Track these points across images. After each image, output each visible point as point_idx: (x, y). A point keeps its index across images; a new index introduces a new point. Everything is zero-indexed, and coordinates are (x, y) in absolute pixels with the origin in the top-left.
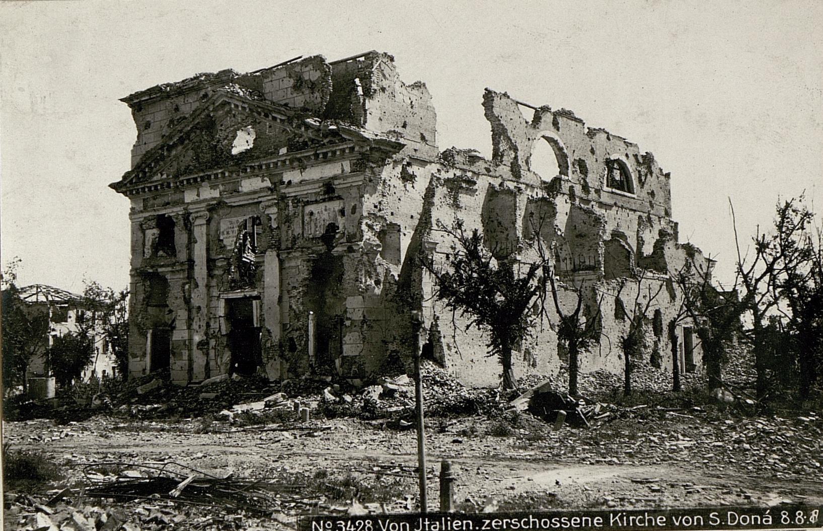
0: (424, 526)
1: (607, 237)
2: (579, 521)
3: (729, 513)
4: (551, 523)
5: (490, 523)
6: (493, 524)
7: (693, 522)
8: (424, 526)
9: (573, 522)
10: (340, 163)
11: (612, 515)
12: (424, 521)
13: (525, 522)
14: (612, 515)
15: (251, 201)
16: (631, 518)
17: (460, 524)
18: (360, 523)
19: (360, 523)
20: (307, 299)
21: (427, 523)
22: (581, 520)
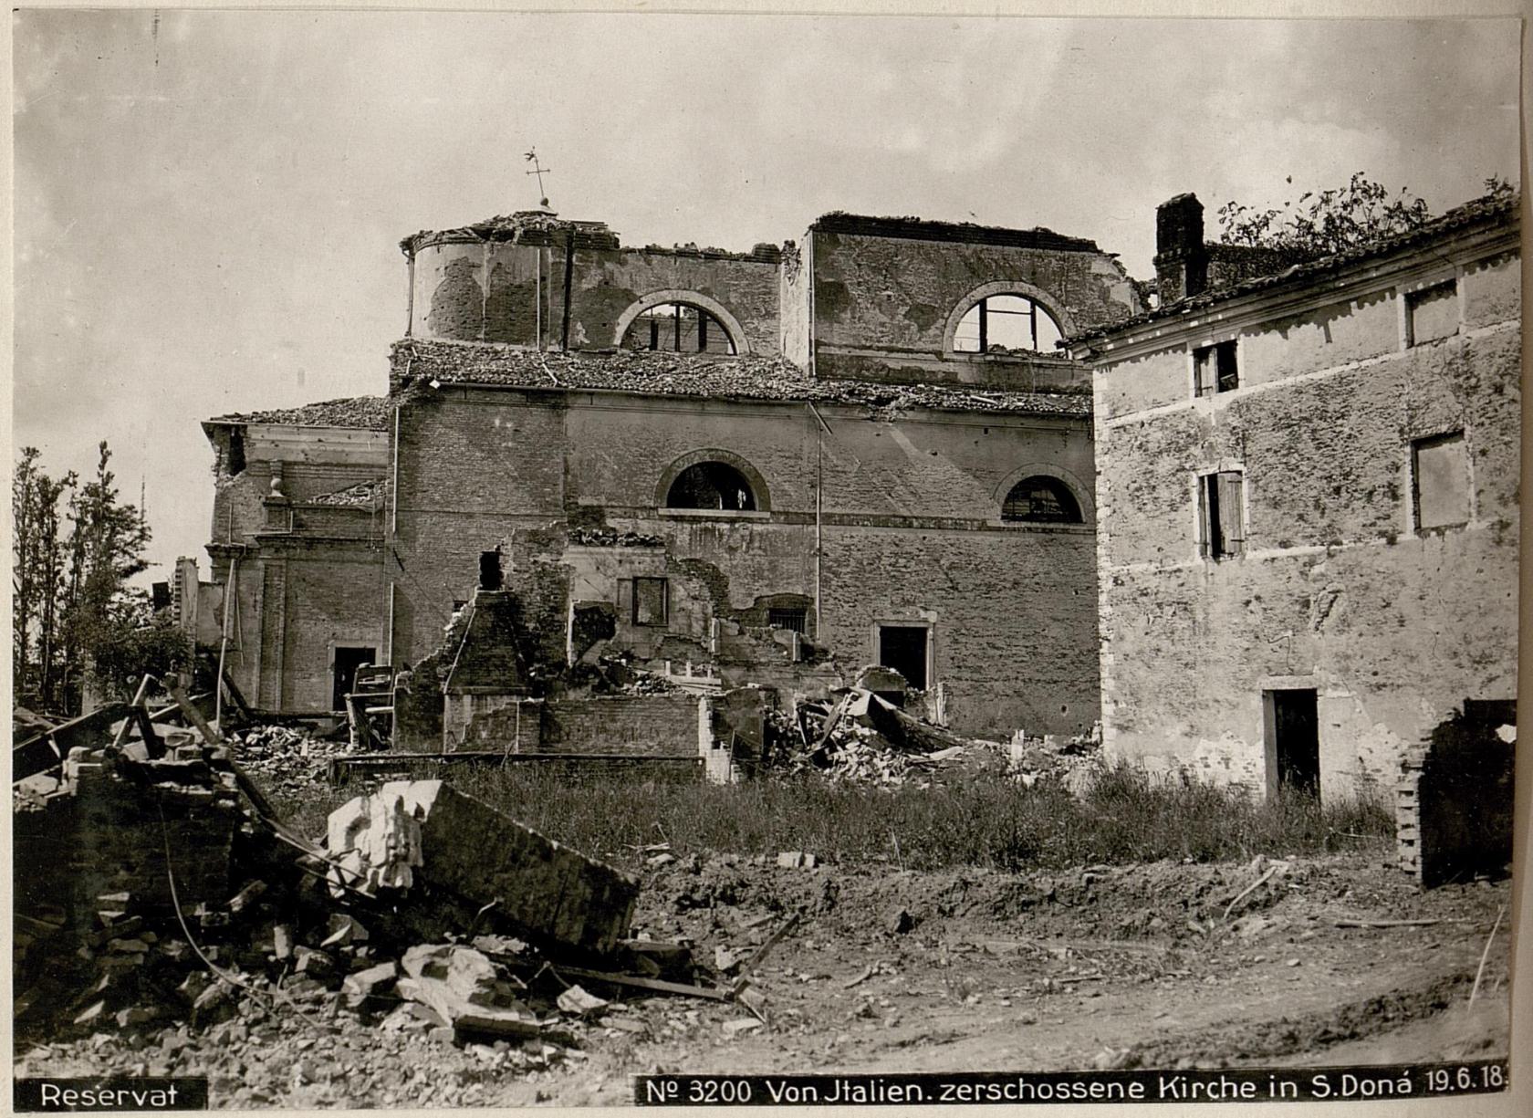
0: (842, 1092)
1: (1513, 229)
2: (112, 1096)
3: (1344, 1077)
4: (1055, 1091)
5: (955, 1090)
6: (959, 1091)
7: (801, 1096)
8: (842, 1092)
9: (1092, 1089)
10: (1416, 791)
11: (1162, 1080)
12: (842, 1085)
13: (1010, 1089)
14: (1162, 1080)
15: (915, 356)
16: (1283, 1085)
17: (1103, 1089)
18: (711, 1086)
19: (711, 1086)
20: (1140, 781)
21: (847, 1088)
22: (904, 1090)
